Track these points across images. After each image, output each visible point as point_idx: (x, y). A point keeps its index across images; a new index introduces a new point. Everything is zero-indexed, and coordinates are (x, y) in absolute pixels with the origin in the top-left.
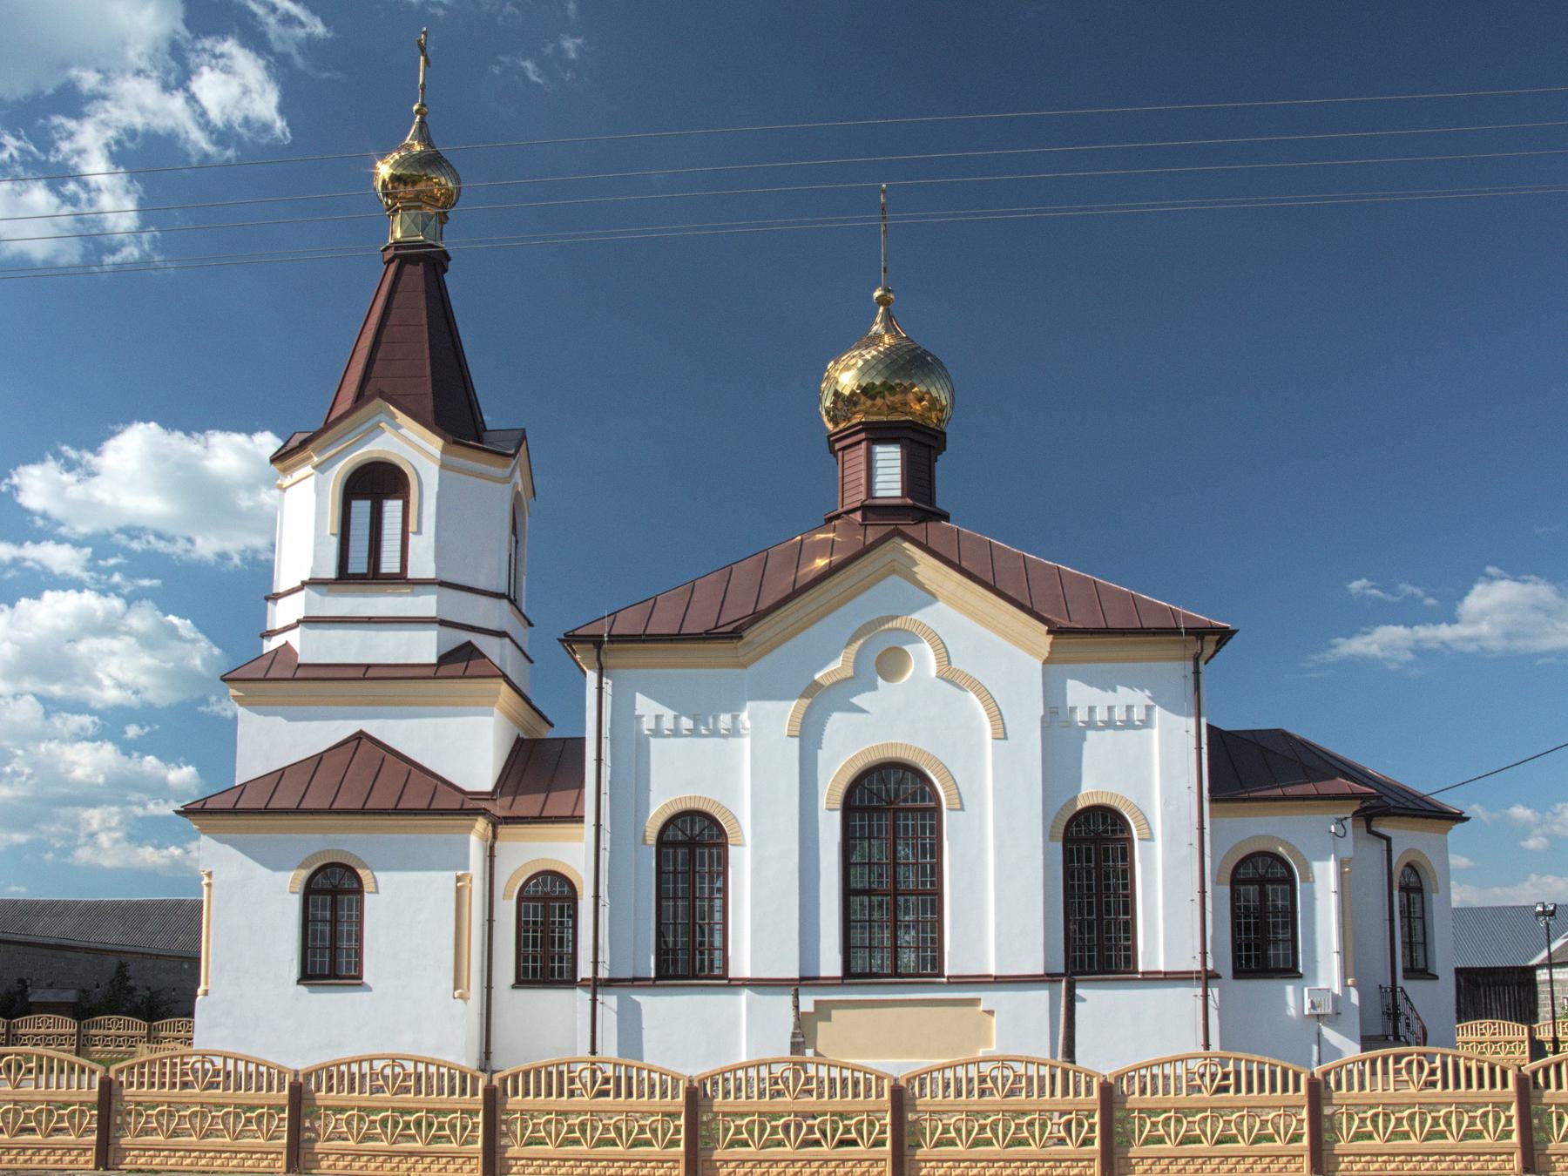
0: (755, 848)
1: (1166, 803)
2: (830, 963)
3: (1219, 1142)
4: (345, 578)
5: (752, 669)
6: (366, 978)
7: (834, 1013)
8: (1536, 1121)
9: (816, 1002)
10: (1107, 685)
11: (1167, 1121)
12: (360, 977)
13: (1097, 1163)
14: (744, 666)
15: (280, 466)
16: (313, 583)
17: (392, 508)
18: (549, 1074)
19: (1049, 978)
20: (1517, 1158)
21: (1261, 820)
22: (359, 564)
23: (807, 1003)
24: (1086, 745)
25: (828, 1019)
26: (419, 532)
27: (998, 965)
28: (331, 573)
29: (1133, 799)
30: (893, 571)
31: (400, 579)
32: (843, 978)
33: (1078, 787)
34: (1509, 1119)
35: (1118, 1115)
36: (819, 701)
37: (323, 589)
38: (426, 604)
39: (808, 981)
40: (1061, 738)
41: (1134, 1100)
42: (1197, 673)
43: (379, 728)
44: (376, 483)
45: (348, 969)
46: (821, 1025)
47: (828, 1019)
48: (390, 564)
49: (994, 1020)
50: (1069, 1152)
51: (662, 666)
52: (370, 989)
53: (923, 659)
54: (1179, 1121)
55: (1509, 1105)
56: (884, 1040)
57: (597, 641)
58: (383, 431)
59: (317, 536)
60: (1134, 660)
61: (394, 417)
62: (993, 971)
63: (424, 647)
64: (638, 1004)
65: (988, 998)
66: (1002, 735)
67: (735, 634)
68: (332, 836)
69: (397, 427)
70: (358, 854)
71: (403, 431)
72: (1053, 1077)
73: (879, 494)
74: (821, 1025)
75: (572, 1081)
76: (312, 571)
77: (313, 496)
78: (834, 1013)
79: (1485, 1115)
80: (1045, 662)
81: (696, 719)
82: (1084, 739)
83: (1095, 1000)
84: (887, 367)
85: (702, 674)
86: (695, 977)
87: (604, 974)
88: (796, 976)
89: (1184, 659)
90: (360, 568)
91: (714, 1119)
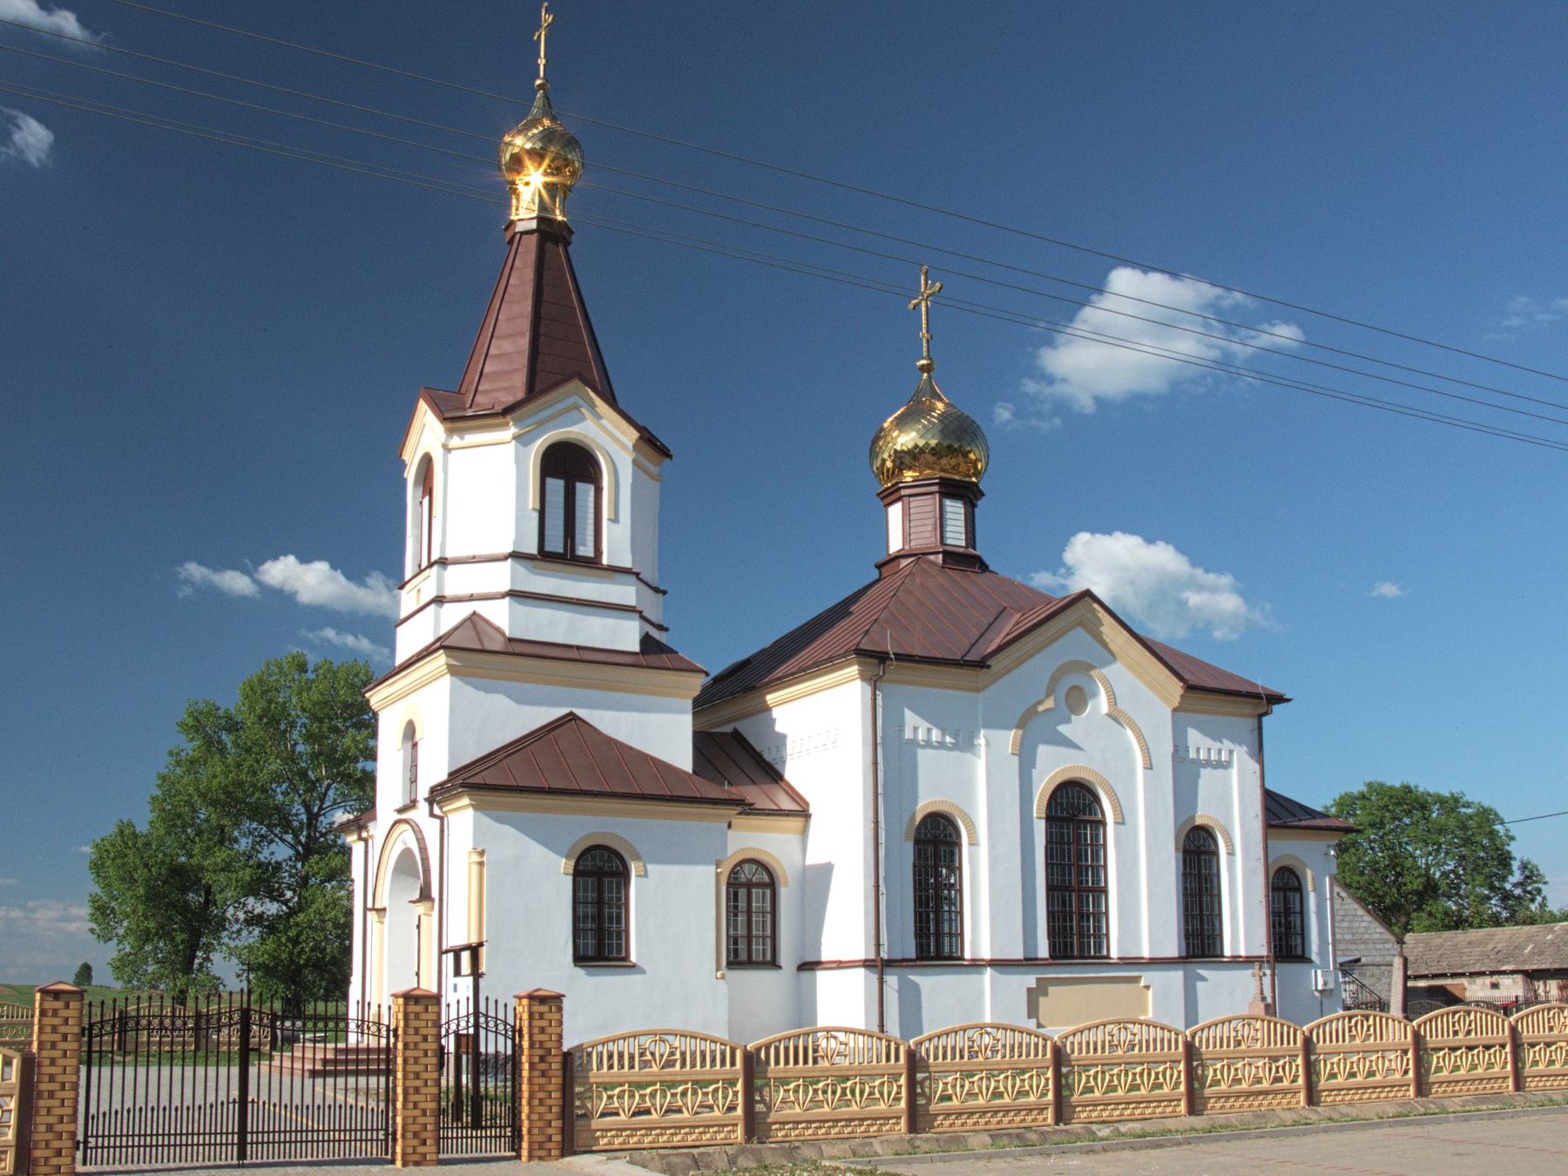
0: (992, 847)
1: (1243, 826)
2: (1043, 951)
3: (634, 1114)
4: (544, 557)
5: (986, 693)
6: (633, 958)
7: (1051, 990)
8: (578, 1103)
9: (1038, 980)
10: (1217, 738)
11: (653, 1095)
12: (627, 958)
13: (903, 1121)
14: (978, 690)
15: (450, 425)
16: (515, 555)
17: (585, 491)
18: (777, 1049)
19: (867, 964)
20: (1510, 1082)
21: (1287, 843)
22: (556, 544)
23: (1030, 980)
24: (1201, 781)
25: (1046, 994)
26: (615, 520)
27: (1151, 950)
28: (533, 549)
29: (1222, 821)
30: (1080, 624)
31: (592, 564)
32: (918, 958)
33: (1195, 809)
34: (735, 1093)
35: (758, 1082)
36: (1034, 728)
37: (529, 564)
38: (626, 593)
39: (1029, 962)
40: (1186, 772)
41: (595, 1075)
42: (1260, 728)
43: (581, 713)
44: (568, 465)
45: (610, 952)
46: (1041, 999)
47: (1046, 994)
48: (585, 550)
49: (1150, 993)
50: (684, 1120)
51: (937, 686)
52: (643, 972)
53: (1102, 703)
54: (695, 1093)
55: (733, 1083)
56: (1075, 1010)
57: (882, 657)
58: (583, 418)
59: (518, 509)
60: (1214, 713)
61: (592, 406)
62: (1146, 954)
63: (626, 636)
64: (917, 986)
65: (1147, 977)
66: (1149, 767)
67: (982, 664)
68: (601, 819)
69: (598, 417)
70: (629, 837)
71: (604, 422)
72: (1045, 1046)
73: (949, 541)
74: (1041, 999)
75: (815, 1051)
76: (515, 542)
77: (513, 468)
78: (1051, 990)
79: (716, 1090)
80: (1175, 710)
81: (955, 735)
82: (1198, 776)
83: (935, 986)
84: (941, 431)
85: (950, 695)
86: (609, 959)
87: (884, 955)
88: (1020, 956)
89: (1249, 716)
90: (559, 548)
91: (1072, 1072)
